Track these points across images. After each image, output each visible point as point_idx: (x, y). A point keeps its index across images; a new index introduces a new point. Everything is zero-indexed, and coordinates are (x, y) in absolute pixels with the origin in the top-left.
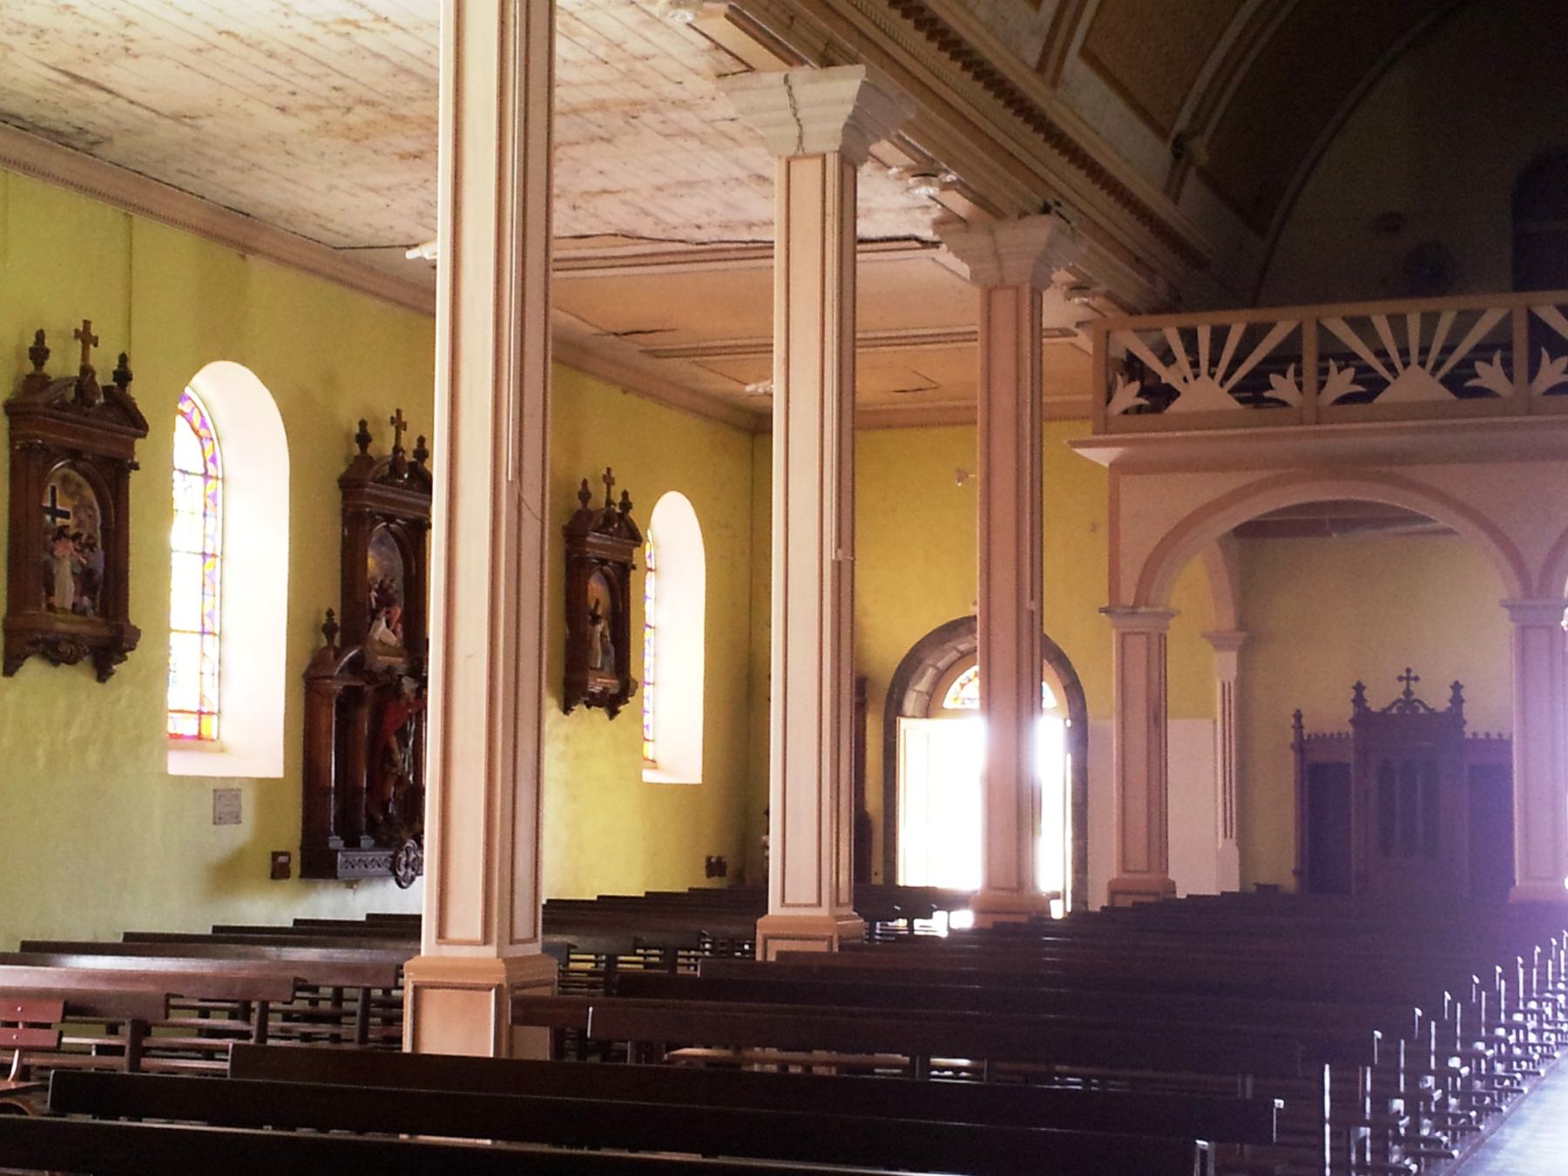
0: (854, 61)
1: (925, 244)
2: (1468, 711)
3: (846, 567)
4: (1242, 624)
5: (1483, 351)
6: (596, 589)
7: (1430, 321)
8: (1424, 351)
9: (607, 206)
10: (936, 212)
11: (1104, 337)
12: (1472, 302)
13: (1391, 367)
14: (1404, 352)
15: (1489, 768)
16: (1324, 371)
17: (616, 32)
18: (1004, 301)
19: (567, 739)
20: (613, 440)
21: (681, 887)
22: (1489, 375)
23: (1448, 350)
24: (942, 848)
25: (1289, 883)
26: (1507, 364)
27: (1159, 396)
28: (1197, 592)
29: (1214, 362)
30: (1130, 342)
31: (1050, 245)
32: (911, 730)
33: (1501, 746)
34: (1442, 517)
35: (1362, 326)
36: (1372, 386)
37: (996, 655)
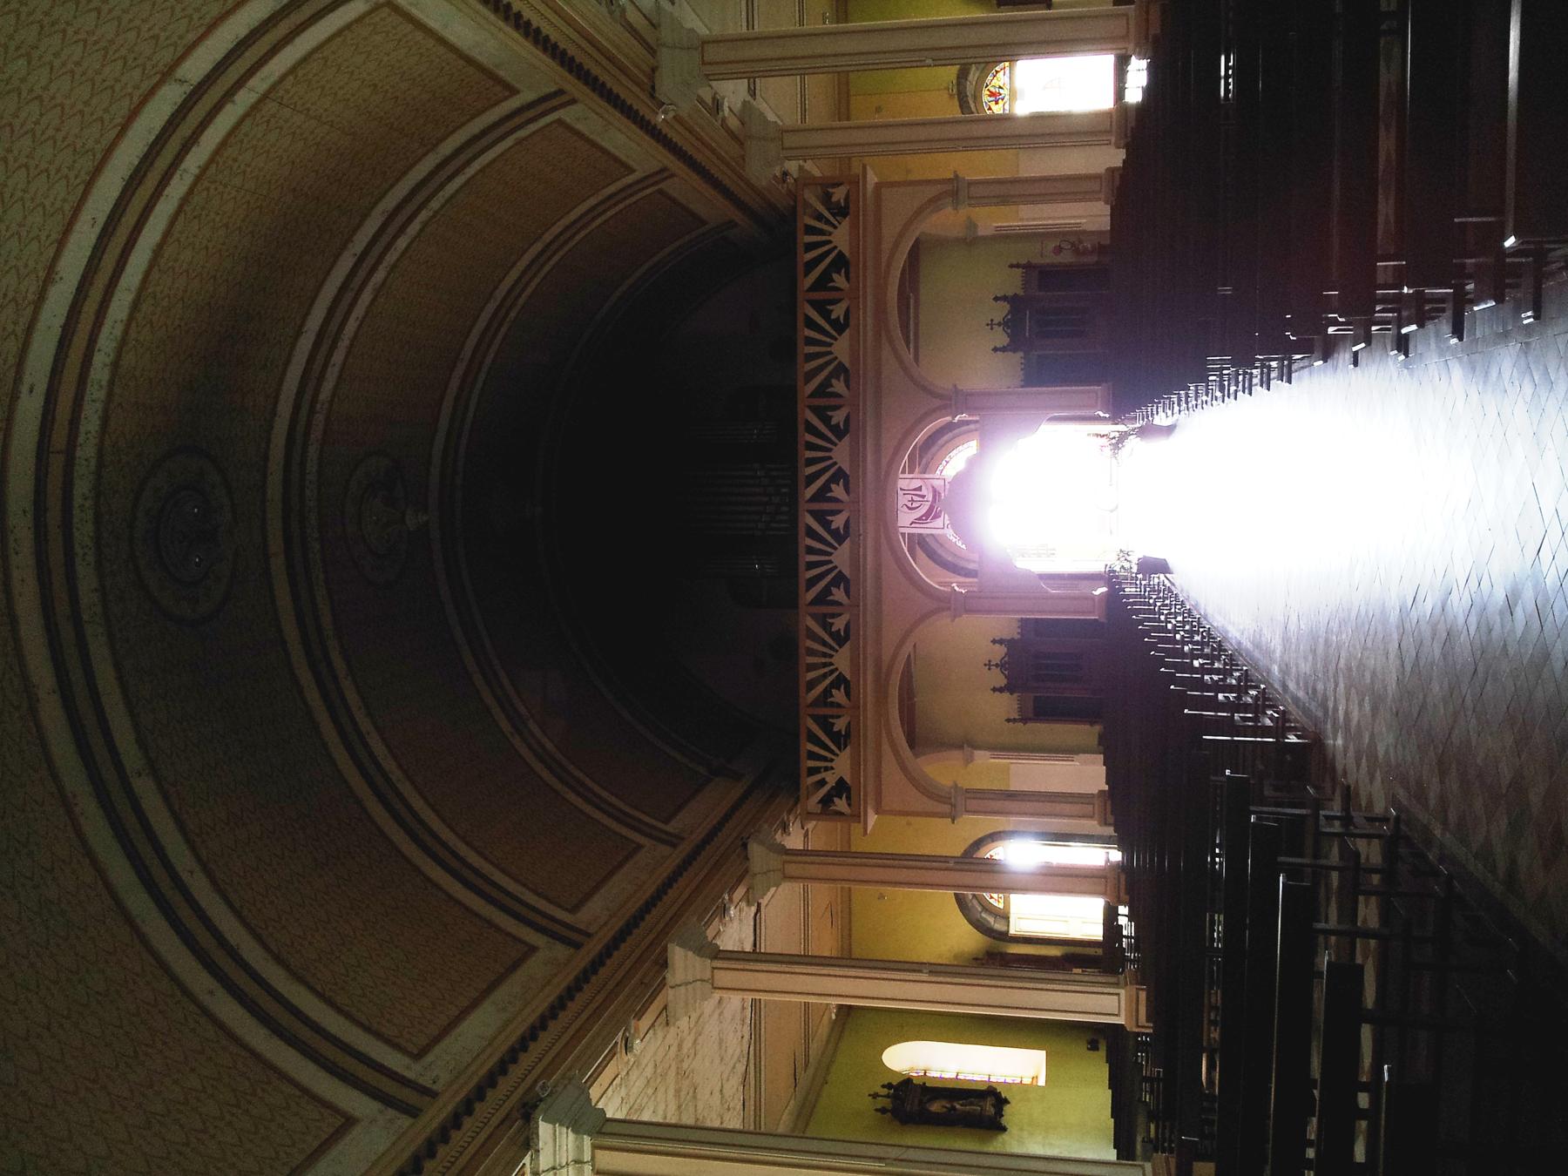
0: (665, 950)
1: (758, 910)
2: (1006, 636)
3: (933, 968)
4: (961, 747)
5: (826, 626)
6: (936, 1107)
7: (811, 652)
8: (825, 655)
9: (728, 1092)
10: (743, 904)
11: (809, 815)
12: (802, 633)
13: (832, 672)
14: (825, 665)
15: (1035, 629)
16: (832, 704)
17: (640, 1083)
18: (792, 869)
19: (1021, 1129)
20: (852, 1097)
21: (1106, 1069)
22: (839, 624)
23: (825, 644)
24: (1080, 918)
25: (1097, 728)
26: (833, 616)
27: (842, 788)
28: (942, 770)
29: (825, 759)
30: (813, 803)
31: (762, 843)
32: (1017, 927)
33: (1024, 623)
34: (907, 649)
35: (811, 685)
36: (841, 681)
37: (979, 883)
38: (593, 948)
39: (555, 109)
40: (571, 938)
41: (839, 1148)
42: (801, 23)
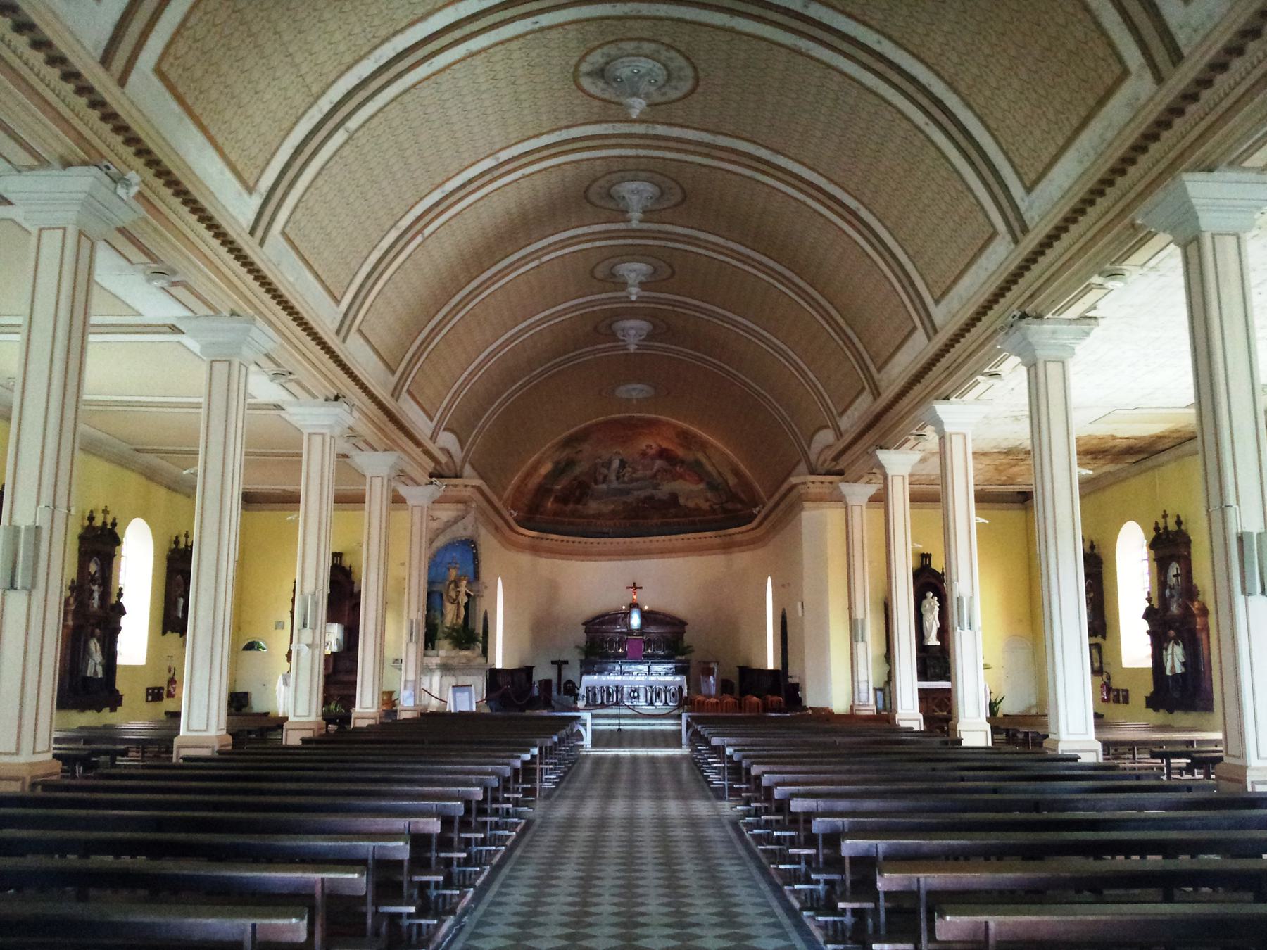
38: (249, 246)
39: (923, 324)
40: (260, 226)
41: (64, 477)
42: (254, 926)
